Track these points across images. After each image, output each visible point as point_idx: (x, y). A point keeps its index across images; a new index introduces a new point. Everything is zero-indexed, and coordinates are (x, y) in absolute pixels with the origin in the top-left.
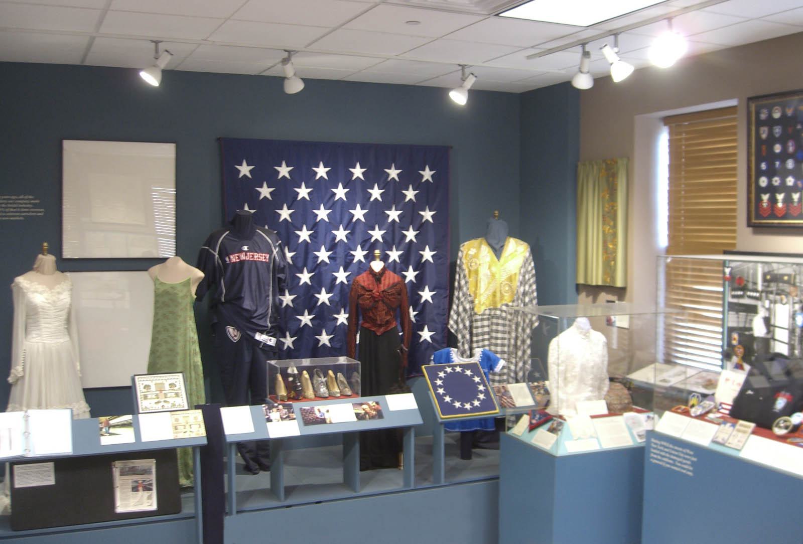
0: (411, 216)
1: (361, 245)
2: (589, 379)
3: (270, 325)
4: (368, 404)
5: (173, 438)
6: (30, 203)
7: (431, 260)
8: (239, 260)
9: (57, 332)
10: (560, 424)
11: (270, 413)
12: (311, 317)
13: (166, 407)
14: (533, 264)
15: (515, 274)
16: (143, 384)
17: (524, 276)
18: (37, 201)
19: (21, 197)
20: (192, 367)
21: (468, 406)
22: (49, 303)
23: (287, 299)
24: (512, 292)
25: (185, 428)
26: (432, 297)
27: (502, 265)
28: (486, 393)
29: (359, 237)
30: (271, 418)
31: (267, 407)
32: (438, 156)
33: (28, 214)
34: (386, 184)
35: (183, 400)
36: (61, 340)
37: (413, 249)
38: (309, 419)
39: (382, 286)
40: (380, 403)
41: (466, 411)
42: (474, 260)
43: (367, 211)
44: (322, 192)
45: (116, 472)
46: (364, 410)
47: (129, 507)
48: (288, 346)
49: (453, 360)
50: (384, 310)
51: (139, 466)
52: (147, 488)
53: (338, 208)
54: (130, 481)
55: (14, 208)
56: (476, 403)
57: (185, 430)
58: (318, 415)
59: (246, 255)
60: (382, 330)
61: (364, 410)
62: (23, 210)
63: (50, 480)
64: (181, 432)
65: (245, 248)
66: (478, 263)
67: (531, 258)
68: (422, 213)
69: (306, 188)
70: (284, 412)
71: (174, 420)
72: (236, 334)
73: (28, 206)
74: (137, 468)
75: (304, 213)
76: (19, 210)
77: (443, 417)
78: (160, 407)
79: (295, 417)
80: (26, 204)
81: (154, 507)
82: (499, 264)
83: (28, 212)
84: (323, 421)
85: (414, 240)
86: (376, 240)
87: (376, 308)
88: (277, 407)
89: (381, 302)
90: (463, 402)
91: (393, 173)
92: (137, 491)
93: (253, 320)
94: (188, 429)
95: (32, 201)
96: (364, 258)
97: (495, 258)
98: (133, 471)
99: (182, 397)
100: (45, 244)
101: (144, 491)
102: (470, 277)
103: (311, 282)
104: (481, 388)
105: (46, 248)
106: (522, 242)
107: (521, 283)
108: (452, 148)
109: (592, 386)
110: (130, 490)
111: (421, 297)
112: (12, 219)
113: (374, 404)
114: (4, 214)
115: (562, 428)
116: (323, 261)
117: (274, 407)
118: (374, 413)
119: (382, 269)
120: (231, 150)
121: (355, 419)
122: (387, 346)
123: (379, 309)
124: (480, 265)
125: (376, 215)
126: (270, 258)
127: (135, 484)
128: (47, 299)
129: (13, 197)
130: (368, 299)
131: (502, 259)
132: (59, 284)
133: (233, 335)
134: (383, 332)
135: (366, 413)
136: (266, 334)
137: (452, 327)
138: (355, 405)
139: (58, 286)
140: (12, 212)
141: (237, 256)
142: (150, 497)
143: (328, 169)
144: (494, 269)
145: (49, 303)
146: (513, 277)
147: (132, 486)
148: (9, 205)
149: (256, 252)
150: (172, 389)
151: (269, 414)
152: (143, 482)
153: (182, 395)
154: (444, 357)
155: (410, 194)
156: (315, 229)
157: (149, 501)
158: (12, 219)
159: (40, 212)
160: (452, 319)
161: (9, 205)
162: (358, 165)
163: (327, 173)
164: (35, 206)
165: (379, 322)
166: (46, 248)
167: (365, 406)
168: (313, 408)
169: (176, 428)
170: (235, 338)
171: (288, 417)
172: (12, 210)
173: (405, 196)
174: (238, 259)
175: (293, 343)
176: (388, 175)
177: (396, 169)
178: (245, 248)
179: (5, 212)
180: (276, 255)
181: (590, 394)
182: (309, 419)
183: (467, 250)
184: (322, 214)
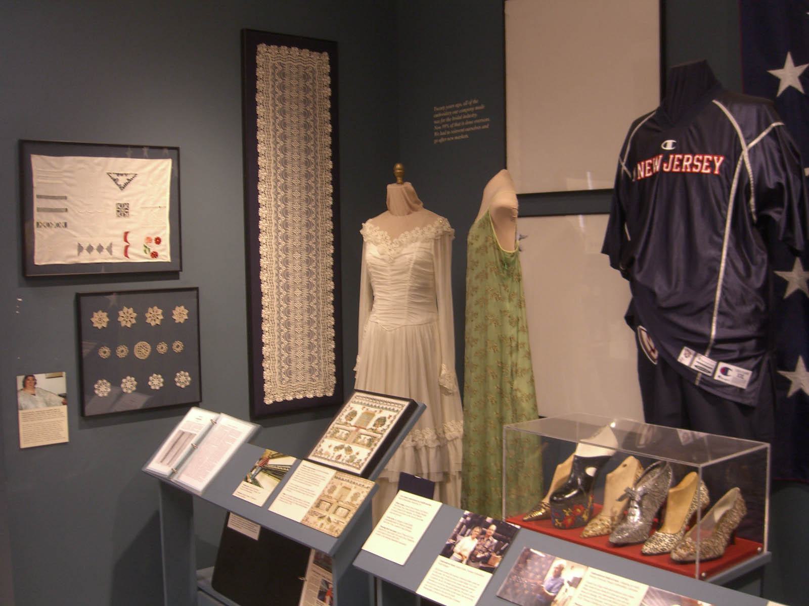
9: (395, 307)
18: (482, 107)
19: (465, 104)
20: (507, 400)
22: (383, 259)
36: (403, 322)
54: (320, 578)
55: (458, 121)
59: (665, 160)
62: (467, 123)
63: (255, 535)
65: (669, 145)
83: (472, 126)
95: (477, 108)
100: (398, 166)
105: (398, 171)
110: (317, 593)
112: (456, 138)
126: (728, 170)
128: (382, 254)
129: (458, 106)
133: (649, 349)
136: (711, 357)
139: (407, 233)
145: (383, 259)
148: (454, 118)
151: (459, 537)
158: (456, 138)
159: (485, 123)
161: (454, 118)
164: (481, 114)
166: (398, 171)
178: (669, 145)
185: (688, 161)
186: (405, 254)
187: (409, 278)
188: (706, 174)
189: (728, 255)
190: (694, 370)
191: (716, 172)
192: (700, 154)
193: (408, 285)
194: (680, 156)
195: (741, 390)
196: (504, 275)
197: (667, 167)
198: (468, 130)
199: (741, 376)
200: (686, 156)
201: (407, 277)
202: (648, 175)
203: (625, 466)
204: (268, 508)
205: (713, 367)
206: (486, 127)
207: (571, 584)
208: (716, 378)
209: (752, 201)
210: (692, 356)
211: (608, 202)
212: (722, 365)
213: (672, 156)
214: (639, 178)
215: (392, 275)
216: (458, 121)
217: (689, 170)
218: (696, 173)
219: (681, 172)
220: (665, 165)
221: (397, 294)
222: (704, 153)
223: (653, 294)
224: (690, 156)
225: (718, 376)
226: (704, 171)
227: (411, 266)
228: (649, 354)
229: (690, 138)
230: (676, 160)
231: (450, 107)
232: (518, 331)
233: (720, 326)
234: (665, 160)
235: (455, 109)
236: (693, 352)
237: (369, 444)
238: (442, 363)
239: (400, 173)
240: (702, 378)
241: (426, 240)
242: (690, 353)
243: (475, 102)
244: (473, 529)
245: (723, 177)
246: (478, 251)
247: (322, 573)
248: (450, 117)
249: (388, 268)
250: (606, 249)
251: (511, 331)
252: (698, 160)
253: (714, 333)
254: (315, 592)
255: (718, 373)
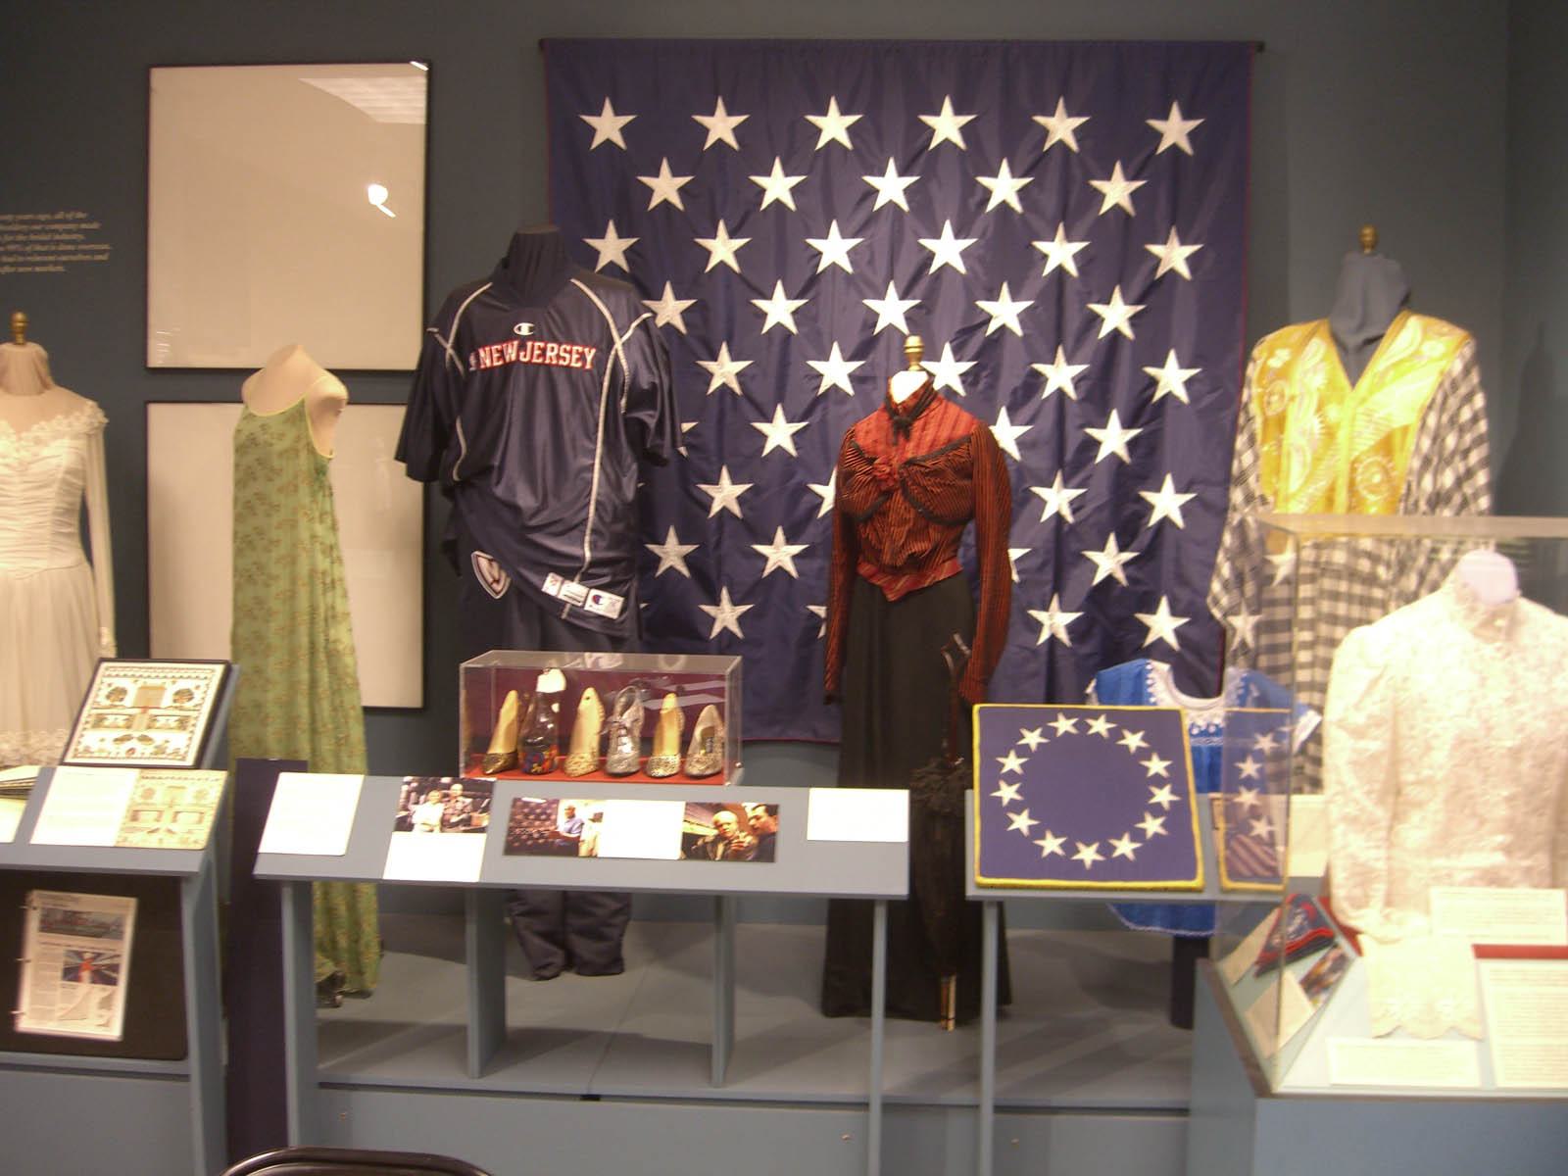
0: (1117, 254)
1: (951, 342)
2: (1496, 799)
3: (588, 554)
4: (738, 810)
5: (112, 845)
6: (79, 231)
7: (1182, 395)
8: (501, 363)
10: (1341, 964)
11: (417, 803)
12: (797, 549)
13: (137, 754)
14: (1479, 401)
15: (1405, 429)
16: (198, 687)
17: (1437, 438)
18: (95, 226)
19: (60, 216)
20: (322, 656)
21: (1088, 854)
23: (725, 493)
24: (1394, 489)
25: (158, 820)
26: (1185, 510)
27: (1364, 400)
28: (1177, 816)
29: (948, 320)
30: (415, 819)
31: (414, 785)
32: (1216, 75)
33: (73, 258)
34: (1036, 161)
35: (190, 739)
36: (42, 564)
37: (1125, 357)
38: (529, 837)
39: (911, 445)
40: (781, 811)
41: (1077, 870)
42: (1279, 385)
43: (975, 240)
44: (833, 187)
45: (33, 921)
46: (718, 826)
47: (51, 1020)
48: (725, 629)
49: (1150, 690)
50: (905, 521)
51: (89, 913)
52: (104, 977)
53: (883, 229)
54: (61, 950)
55: (43, 243)
56: (1125, 847)
57: (155, 825)
58: (562, 825)
59: (522, 347)
60: (902, 584)
61: (718, 826)
62: (62, 248)
64: (140, 830)
65: (524, 329)
66: (1288, 393)
67: (1475, 378)
68: (1156, 249)
69: (600, 115)
70: (459, 806)
71: (140, 791)
72: (497, 576)
73: (74, 237)
74: (85, 916)
75: (779, 247)
76: (53, 248)
77: (1230, 884)
78: (123, 754)
79: (485, 823)
80: (69, 232)
81: (114, 1031)
82: (1352, 397)
84: (569, 847)
85: (1127, 331)
86: (1003, 329)
87: (884, 514)
88: (448, 787)
89: (898, 497)
90: (1074, 837)
91: (1061, 127)
92: (77, 979)
93: (530, 536)
94: (166, 822)
95: (84, 226)
96: (963, 382)
97: (1342, 380)
98: (69, 924)
99: (192, 732)
100: (19, 316)
101: (94, 982)
102: (1264, 442)
103: (797, 449)
104: (1163, 796)
106: (1445, 327)
107: (1426, 461)
108: (1261, 47)
109: (1510, 825)
110: (60, 974)
111: (1149, 508)
112: (38, 269)
113: (760, 811)
114: (21, 259)
115: (1338, 981)
116: (835, 388)
117: (436, 786)
118: (748, 840)
119: (915, 395)
120: (575, 70)
121: (674, 851)
122: (891, 639)
123: (892, 517)
124: (1292, 398)
125: (1005, 252)
126: (599, 362)
127: (76, 961)
129: (43, 217)
130: (864, 484)
131: (1366, 381)
132: (48, 417)
133: (490, 580)
134: (904, 592)
135: (721, 837)
136: (582, 581)
137: (1216, 602)
138: (694, 807)
139: (43, 423)
140: (40, 253)
141: (498, 351)
142: (106, 1004)
143: (851, 119)
144: (1333, 412)
146: (1397, 440)
147: (66, 963)
148: (33, 237)
149: (555, 340)
150: (177, 704)
151: (412, 807)
152: (94, 959)
153: (194, 725)
154: (1127, 687)
155: (1117, 191)
156: (812, 294)
157: (103, 1012)
158: (38, 269)
159: (102, 252)
160: (1219, 575)
161: (33, 237)
162: (947, 107)
163: (851, 130)
164: (91, 236)
165: (887, 558)
166: (21, 324)
167: (724, 817)
168: (557, 802)
169: (135, 816)
170: (498, 587)
171: (467, 822)
172: (39, 248)
173: (1100, 196)
174: (499, 359)
175: (741, 620)
176: (1045, 132)
177: (1071, 113)
178: (524, 329)
179: (23, 254)
180: (621, 354)
181: (1499, 858)
182: (529, 837)
183: (1265, 354)
184: (835, 249)
185: (553, 351)
186: (48, 457)
187: (53, 495)
188: (577, 368)
189: (601, 464)
190: (561, 600)
191: (588, 366)
192: (567, 343)
193: (51, 505)
194: (542, 345)
195: (611, 620)
196: (316, 488)
197: (525, 356)
198: (64, 258)
199: (613, 605)
200: (550, 346)
201: (51, 492)
202: (496, 364)
203: (588, 698)
204: (29, 840)
205: (584, 595)
206: (104, 257)
207: (593, 820)
208: (587, 608)
209: (623, 402)
210: (558, 584)
211: (406, 389)
212: (594, 592)
213: (529, 344)
214: (483, 367)
215: (25, 490)
216: (43, 243)
217: (554, 362)
218: (562, 366)
219: (543, 364)
220: (522, 354)
221: (32, 520)
222: (573, 343)
223: (515, 509)
224: (555, 346)
225: (590, 606)
226: (573, 364)
227: (60, 476)
228: (490, 586)
229: (550, 321)
230: (536, 348)
231: (27, 217)
232: (332, 563)
233: (594, 547)
234: (522, 347)
235: (38, 222)
236: (560, 579)
237: (183, 723)
238: (99, 625)
239: (23, 327)
240: (571, 609)
241: (76, 437)
242: (556, 581)
243: (80, 215)
244: (427, 794)
245: (595, 372)
246: (281, 454)
247: (63, 942)
248: (27, 234)
249: (16, 480)
250: (402, 455)
251: (323, 563)
252: (565, 351)
253: (588, 554)
254: (55, 973)
255: (590, 601)
